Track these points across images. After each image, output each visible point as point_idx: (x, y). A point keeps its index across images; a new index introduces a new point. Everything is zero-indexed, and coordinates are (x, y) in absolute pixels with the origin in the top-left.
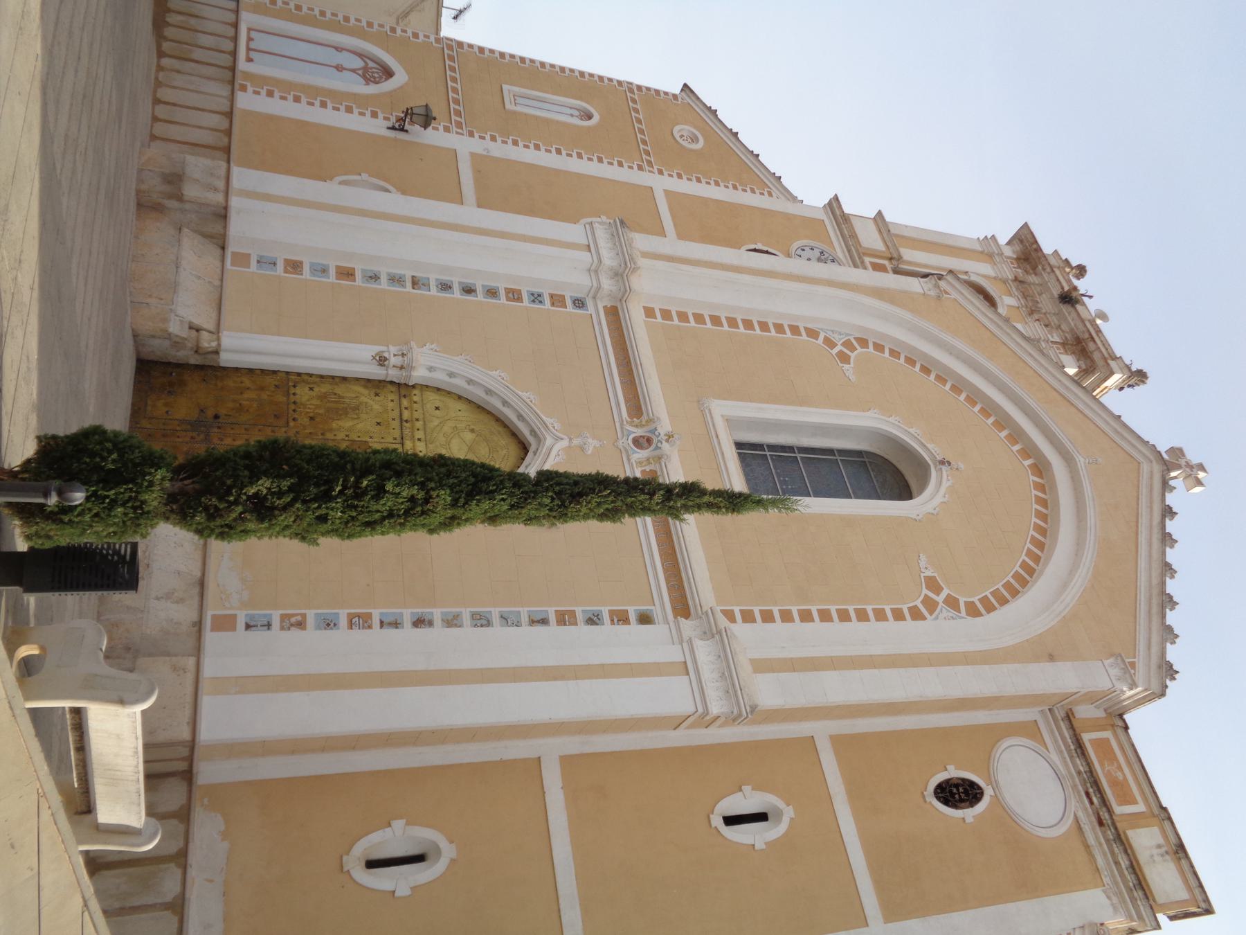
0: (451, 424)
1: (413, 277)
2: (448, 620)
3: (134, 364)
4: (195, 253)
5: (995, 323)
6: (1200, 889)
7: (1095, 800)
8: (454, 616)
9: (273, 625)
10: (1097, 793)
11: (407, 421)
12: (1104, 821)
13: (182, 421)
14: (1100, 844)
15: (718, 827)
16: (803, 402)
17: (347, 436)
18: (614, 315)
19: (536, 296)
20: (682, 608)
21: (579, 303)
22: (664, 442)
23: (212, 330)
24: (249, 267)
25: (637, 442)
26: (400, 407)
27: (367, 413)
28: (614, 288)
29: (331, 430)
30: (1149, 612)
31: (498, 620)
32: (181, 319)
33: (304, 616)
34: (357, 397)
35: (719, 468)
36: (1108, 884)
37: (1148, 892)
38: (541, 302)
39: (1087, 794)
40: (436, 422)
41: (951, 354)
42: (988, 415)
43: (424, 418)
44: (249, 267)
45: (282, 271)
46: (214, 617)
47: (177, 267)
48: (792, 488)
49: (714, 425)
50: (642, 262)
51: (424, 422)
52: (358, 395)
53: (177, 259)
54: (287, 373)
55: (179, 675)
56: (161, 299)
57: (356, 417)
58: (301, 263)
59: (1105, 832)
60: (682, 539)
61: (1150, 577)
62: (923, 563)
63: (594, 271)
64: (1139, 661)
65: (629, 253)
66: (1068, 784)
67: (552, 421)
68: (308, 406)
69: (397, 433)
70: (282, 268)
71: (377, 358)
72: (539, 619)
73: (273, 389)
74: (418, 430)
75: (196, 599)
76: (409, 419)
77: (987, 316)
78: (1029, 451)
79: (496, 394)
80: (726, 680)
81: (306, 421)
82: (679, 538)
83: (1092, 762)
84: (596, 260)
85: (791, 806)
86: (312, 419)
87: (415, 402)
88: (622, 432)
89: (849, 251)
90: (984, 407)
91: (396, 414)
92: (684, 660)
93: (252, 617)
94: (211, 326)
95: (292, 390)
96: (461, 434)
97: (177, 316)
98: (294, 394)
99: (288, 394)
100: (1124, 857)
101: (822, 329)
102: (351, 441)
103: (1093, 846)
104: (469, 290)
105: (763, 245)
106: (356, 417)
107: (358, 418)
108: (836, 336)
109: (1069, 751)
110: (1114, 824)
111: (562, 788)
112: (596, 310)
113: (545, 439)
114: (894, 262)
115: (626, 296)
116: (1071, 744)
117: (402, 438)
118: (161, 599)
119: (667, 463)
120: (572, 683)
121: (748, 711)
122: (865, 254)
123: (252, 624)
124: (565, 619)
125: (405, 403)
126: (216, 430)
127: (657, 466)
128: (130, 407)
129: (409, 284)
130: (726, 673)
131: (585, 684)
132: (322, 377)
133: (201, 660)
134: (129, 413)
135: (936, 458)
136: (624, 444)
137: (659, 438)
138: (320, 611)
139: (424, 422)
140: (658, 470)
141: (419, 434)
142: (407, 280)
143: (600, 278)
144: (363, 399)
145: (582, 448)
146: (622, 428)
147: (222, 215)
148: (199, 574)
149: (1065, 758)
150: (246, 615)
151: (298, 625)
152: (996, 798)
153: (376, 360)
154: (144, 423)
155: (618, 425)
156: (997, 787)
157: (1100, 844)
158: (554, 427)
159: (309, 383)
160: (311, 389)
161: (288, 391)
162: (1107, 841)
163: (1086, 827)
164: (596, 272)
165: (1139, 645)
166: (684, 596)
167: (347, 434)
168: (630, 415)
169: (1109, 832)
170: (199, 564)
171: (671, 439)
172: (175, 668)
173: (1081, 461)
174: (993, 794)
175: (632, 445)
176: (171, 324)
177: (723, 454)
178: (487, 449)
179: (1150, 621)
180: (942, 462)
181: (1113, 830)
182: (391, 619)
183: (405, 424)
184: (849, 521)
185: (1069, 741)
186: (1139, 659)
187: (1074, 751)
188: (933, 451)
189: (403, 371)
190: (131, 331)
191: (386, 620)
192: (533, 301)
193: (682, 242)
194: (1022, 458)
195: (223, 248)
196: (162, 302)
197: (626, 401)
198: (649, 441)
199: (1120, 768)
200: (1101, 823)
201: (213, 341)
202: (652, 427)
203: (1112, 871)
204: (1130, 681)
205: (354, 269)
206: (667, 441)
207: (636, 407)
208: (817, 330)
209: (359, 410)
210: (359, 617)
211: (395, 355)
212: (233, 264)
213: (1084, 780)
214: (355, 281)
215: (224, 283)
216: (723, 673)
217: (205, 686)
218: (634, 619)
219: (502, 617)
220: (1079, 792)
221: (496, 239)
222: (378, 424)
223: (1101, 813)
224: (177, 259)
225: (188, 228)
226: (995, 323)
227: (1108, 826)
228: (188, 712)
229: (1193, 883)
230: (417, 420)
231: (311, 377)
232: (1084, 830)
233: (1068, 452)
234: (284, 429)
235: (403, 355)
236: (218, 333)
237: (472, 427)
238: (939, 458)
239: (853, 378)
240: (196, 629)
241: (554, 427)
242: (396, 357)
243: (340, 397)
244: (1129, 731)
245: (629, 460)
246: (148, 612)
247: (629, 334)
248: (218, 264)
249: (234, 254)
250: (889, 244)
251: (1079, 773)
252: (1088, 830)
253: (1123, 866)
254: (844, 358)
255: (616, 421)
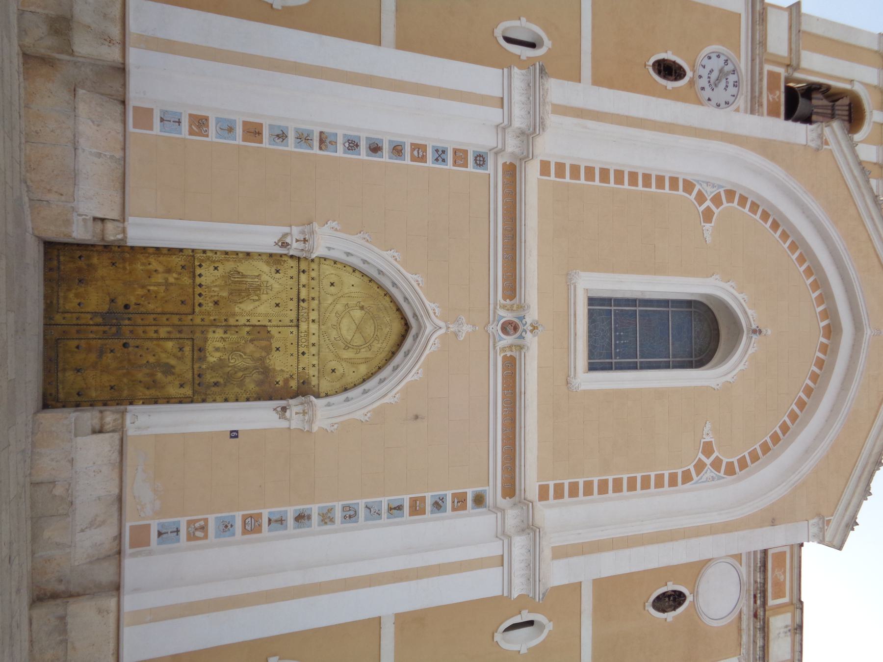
0: (344, 301)
1: (321, 133)
2: (323, 514)
4: (93, 122)
5: (857, 182)
6: (800, 653)
7: (758, 602)
8: (328, 510)
9: (181, 531)
10: (762, 598)
11: (303, 301)
12: (758, 616)
13: (95, 314)
14: (749, 629)
15: (498, 642)
16: (658, 270)
17: (248, 321)
18: (511, 172)
19: (440, 152)
20: (510, 489)
21: (480, 160)
22: (528, 332)
24: (151, 129)
25: (504, 329)
27: (267, 294)
28: (517, 150)
29: (234, 315)
30: (860, 478)
31: (363, 509)
32: (84, 217)
33: (206, 520)
34: (259, 275)
35: (568, 348)
36: (743, 654)
37: (766, 656)
38: (443, 160)
39: (755, 596)
40: (330, 300)
41: (804, 212)
42: (808, 277)
43: (319, 297)
44: (151, 129)
45: (187, 133)
46: (132, 528)
47: (75, 149)
48: (624, 343)
49: (575, 303)
50: (552, 120)
51: (319, 300)
52: (261, 273)
53: (74, 136)
55: (103, 617)
56: (62, 195)
58: (207, 119)
59: (755, 622)
60: (523, 289)
61: (874, 445)
62: (706, 430)
63: (502, 129)
64: (834, 520)
65: (541, 114)
66: (745, 588)
67: (433, 305)
68: (213, 289)
69: (293, 315)
70: (187, 128)
71: (280, 244)
72: (396, 506)
74: (313, 310)
75: (116, 515)
76: (306, 298)
77: (852, 171)
78: (830, 314)
80: (530, 570)
81: (209, 306)
82: (521, 428)
83: (767, 578)
84: (506, 122)
85: (552, 623)
87: (313, 279)
88: (494, 316)
89: (753, 60)
90: (810, 266)
92: (502, 96)
93: (162, 525)
94: (115, 215)
95: (198, 271)
97: (80, 215)
99: (194, 276)
100: (762, 640)
101: (698, 181)
102: (252, 326)
103: (744, 629)
104: (375, 149)
105: (673, 54)
108: (709, 189)
109: (755, 566)
110: (764, 619)
111: (394, 623)
112: (494, 170)
114: (790, 70)
115: (531, 520)
116: (759, 563)
118: (86, 530)
119: (526, 353)
120: (413, 583)
121: (540, 598)
122: (769, 61)
123: (163, 531)
124: (417, 508)
125: (304, 278)
126: (127, 322)
127: (518, 353)
129: (316, 143)
130: (531, 565)
131: (424, 582)
133: (121, 600)
135: (751, 326)
136: (493, 330)
137: (525, 328)
138: (219, 515)
139: (319, 300)
140: (517, 358)
141: (314, 315)
142: (315, 138)
143: (507, 137)
144: (265, 277)
145: (456, 334)
146: (495, 312)
147: (122, 70)
148: (117, 491)
149: (750, 571)
150: (158, 524)
151: (201, 528)
152: (693, 603)
153: (279, 245)
154: (58, 318)
155: (492, 307)
156: (697, 596)
157: (749, 629)
158: (435, 313)
159: (214, 262)
160: (216, 268)
161: (194, 273)
162: (755, 628)
163: (745, 616)
164: (504, 129)
165: (842, 500)
166: (513, 478)
167: (248, 318)
168: (504, 299)
169: (759, 624)
170: (117, 481)
171: (536, 331)
172: (100, 611)
173: (868, 332)
174: (692, 600)
175: (500, 332)
176: (74, 228)
177: (575, 335)
179: (857, 486)
180: (754, 332)
181: (761, 623)
182: (277, 517)
183: (301, 304)
184: (660, 394)
185: (759, 560)
186: (834, 518)
187: (758, 568)
188: (751, 317)
191: (273, 518)
192: (437, 160)
193: (596, 88)
194: (819, 348)
195: (124, 103)
196: (63, 198)
197: (504, 280)
198: (516, 329)
199: (785, 572)
200: (755, 616)
201: (119, 234)
202: (522, 314)
203: (749, 647)
204: (821, 538)
205: (262, 124)
206: (531, 331)
207: (512, 288)
208: (692, 181)
210: (251, 517)
211: (297, 241)
212: (135, 127)
213: (757, 588)
214: (261, 142)
215: (127, 154)
216: (529, 565)
217: (125, 620)
218: (471, 499)
219: (367, 507)
220: (750, 595)
221: (408, 96)
222: (277, 305)
223: (759, 611)
224: (74, 136)
225: (83, 88)
226: (857, 182)
227: (760, 620)
228: (112, 645)
229: (797, 648)
230: (313, 299)
231: (216, 253)
232: (742, 619)
233: (861, 323)
234: (190, 317)
235: (305, 240)
236: (124, 220)
237: (362, 303)
238: (754, 327)
239: (709, 239)
240: (117, 542)
241: (435, 313)
243: (244, 276)
244: (802, 548)
245: (494, 347)
246: (75, 546)
247: (521, 288)
248: (119, 127)
249: (136, 109)
250: (793, 46)
251: (756, 582)
252: (745, 618)
253: (758, 645)
254: (708, 215)
255: (491, 302)
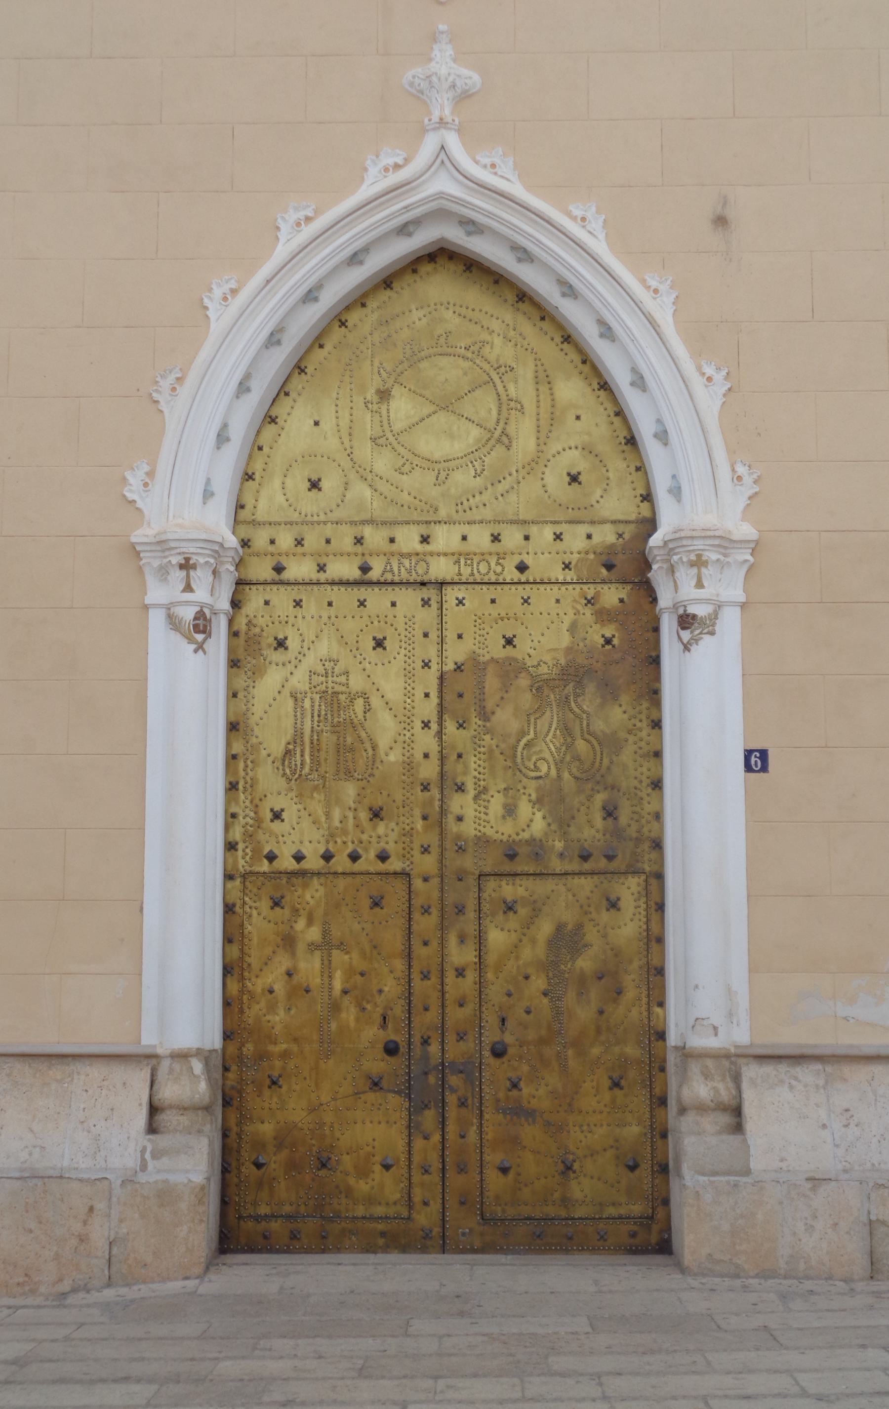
0: (365, 451)
3: (674, 1248)
11: (365, 569)
17: (426, 725)
23: (146, 1074)
26: (318, 583)
29: (409, 766)
32: (148, 1156)
43: (353, 523)
51: (363, 522)
52: (286, 692)
54: (228, 877)
56: (91, 1209)
57: (360, 702)
67: (373, 171)
68: (337, 823)
69: (409, 599)
73: (287, 911)
74: (392, 540)
79: (282, 320)
86: (376, 814)
91: (346, 598)
94: (139, 1079)
95: (287, 863)
96: (398, 426)
98: (299, 857)
106: (360, 702)
107: (365, 696)
113: (441, 195)
117: (423, 584)
126: (434, 1048)
128: (380, 1257)
132: (232, 787)
134: (394, 1257)
139: (363, 522)
141: (408, 538)
144: (299, 681)
145: (463, 97)
153: (205, 640)
154: (425, 1218)
158: (397, 167)
160: (277, 816)
167: (418, 725)
178: (444, 361)
183: (374, 575)
189: (222, 569)
190: (211, 1276)
196: (100, 1206)
209: (336, 693)
222: (379, 644)
230: (359, 541)
234: (418, 883)
237: (371, 394)
241: (397, 167)
242: (194, 586)
